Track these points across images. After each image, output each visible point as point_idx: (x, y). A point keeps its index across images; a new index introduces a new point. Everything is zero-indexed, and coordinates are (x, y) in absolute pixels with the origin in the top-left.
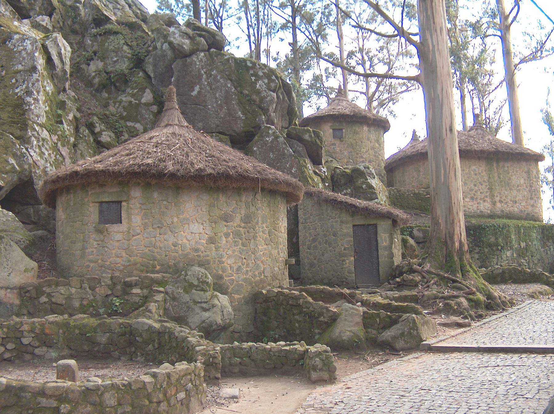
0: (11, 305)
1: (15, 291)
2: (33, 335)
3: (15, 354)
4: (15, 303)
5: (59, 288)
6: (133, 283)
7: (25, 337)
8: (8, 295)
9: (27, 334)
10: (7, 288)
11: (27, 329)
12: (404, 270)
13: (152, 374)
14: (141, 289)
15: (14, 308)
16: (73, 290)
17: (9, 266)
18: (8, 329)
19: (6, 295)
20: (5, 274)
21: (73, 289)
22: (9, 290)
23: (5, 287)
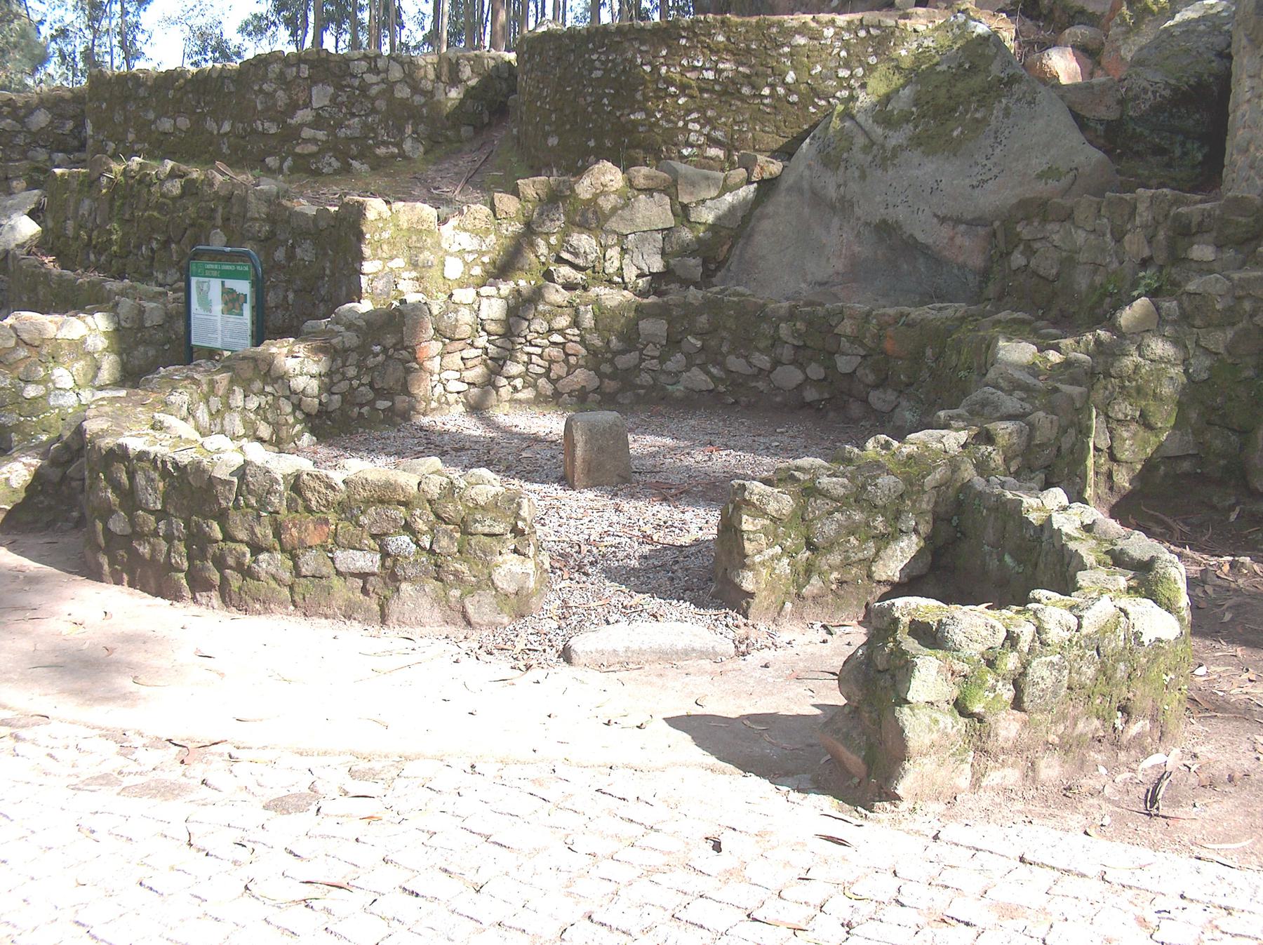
0: (962, 267)
1: (981, 231)
2: (863, 353)
3: (826, 396)
4: (970, 263)
5: (1049, 227)
6: (1196, 219)
7: (843, 354)
8: (958, 240)
9: (847, 344)
10: (958, 221)
11: (848, 331)
12: (767, 522)
13: (50, 659)
14: (1219, 247)
15: (971, 278)
16: (1080, 237)
17: (993, 160)
18: (810, 323)
19: (952, 239)
20: (967, 181)
21: (1080, 232)
22: (962, 227)
23: (951, 219)
